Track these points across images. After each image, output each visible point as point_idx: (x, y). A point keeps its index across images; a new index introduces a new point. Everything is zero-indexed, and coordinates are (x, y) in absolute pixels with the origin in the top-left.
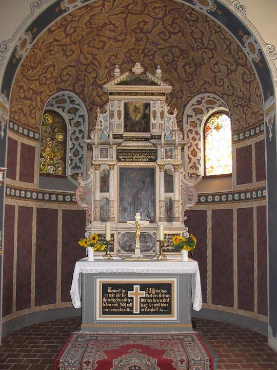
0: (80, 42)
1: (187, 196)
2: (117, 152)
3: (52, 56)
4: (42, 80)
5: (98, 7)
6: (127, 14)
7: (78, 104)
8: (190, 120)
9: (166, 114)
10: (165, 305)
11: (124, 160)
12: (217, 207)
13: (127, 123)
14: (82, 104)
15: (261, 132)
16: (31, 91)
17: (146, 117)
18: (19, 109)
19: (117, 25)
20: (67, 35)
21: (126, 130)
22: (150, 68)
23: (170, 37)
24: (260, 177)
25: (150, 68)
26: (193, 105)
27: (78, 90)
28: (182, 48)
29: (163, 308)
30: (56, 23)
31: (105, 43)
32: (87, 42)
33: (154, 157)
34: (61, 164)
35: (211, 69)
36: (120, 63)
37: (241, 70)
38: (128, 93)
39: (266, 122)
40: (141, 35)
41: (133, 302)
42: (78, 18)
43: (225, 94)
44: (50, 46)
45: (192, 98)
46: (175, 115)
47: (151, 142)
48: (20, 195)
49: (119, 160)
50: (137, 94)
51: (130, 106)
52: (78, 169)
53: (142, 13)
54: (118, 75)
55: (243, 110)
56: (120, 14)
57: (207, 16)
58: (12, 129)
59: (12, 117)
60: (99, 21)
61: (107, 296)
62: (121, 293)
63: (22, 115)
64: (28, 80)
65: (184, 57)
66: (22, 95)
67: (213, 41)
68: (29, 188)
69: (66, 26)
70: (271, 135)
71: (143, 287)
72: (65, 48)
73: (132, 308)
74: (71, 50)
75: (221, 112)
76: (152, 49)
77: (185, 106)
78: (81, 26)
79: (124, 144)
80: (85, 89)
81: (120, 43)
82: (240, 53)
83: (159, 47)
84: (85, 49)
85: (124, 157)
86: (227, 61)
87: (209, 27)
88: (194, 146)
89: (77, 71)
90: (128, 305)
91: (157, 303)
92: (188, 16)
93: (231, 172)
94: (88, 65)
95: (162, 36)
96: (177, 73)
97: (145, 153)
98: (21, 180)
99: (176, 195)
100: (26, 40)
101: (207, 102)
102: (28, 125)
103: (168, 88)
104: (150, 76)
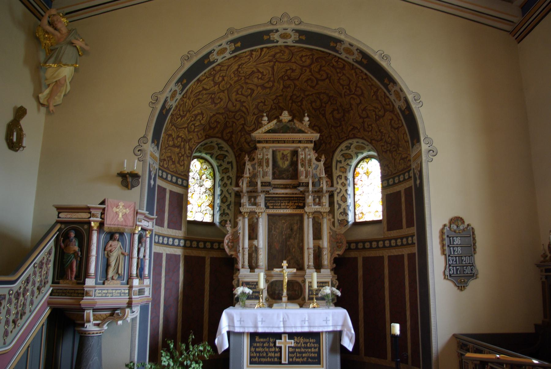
0: (228, 90)
1: (335, 243)
2: (265, 200)
3: (200, 105)
4: (191, 128)
5: (246, 57)
6: (275, 62)
7: (227, 151)
8: (339, 165)
9: (314, 161)
10: (313, 355)
11: (272, 207)
12: (368, 254)
13: (275, 170)
14: (230, 151)
15: (410, 177)
16: (180, 139)
17: (294, 164)
18: (168, 157)
19: (265, 73)
20: (216, 84)
21: (274, 178)
22: (297, 116)
23: (317, 84)
24: (410, 224)
25: (297, 116)
26: (342, 150)
27: (227, 137)
28: (330, 94)
29: (312, 358)
30: (205, 73)
31: (253, 90)
32: (235, 89)
33: (301, 205)
34: (210, 211)
35: (359, 115)
36: (268, 110)
37: (388, 116)
38: (276, 141)
39: (413, 169)
40: (288, 82)
41: (281, 352)
42: (226, 67)
43: (374, 139)
44: (199, 95)
45: (341, 143)
46: (322, 163)
47: (299, 190)
48: (168, 242)
49: (267, 207)
50: (284, 142)
51: (278, 153)
52: (226, 216)
53: (289, 61)
54: (266, 123)
55: (392, 155)
56: (267, 62)
57: (353, 65)
58: (161, 177)
59: (161, 164)
60: (247, 70)
61: (255, 345)
62: (269, 342)
63: (170, 163)
64: (177, 128)
65: (332, 104)
66: (171, 143)
67: (360, 88)
68: (177, 235)
69: (214, 76)
70: (418, 182)
71: (292, 335)
72: (213, 96)
73: (280, 358)
74: (219, 98)
75: (370, 157)
76: (300, 95)
77: (334, 152)
78: (229, 75)
79: (272, 191)
80: (234, 136)
81: (268, 90)
82: (387, 99)
83: (307, 93)
84: (234, 96)
85: (272, 204)
86: (375, 107)
87: (356, 75)
88: (343, 192)
89: (225, 118)
90: (276, 355)
91: (305, 352)
92: (335, 64)
93: (381, 218)
94: (237, 112)
95: (309, 82)
96: (326, 118)
97: (294, 200)
98: (169, 227)
99: (325, 243)
100: (176, 91)
101: (356, 148)
102: (176, 172)
103: (316, 136)
104: (298, 125)
